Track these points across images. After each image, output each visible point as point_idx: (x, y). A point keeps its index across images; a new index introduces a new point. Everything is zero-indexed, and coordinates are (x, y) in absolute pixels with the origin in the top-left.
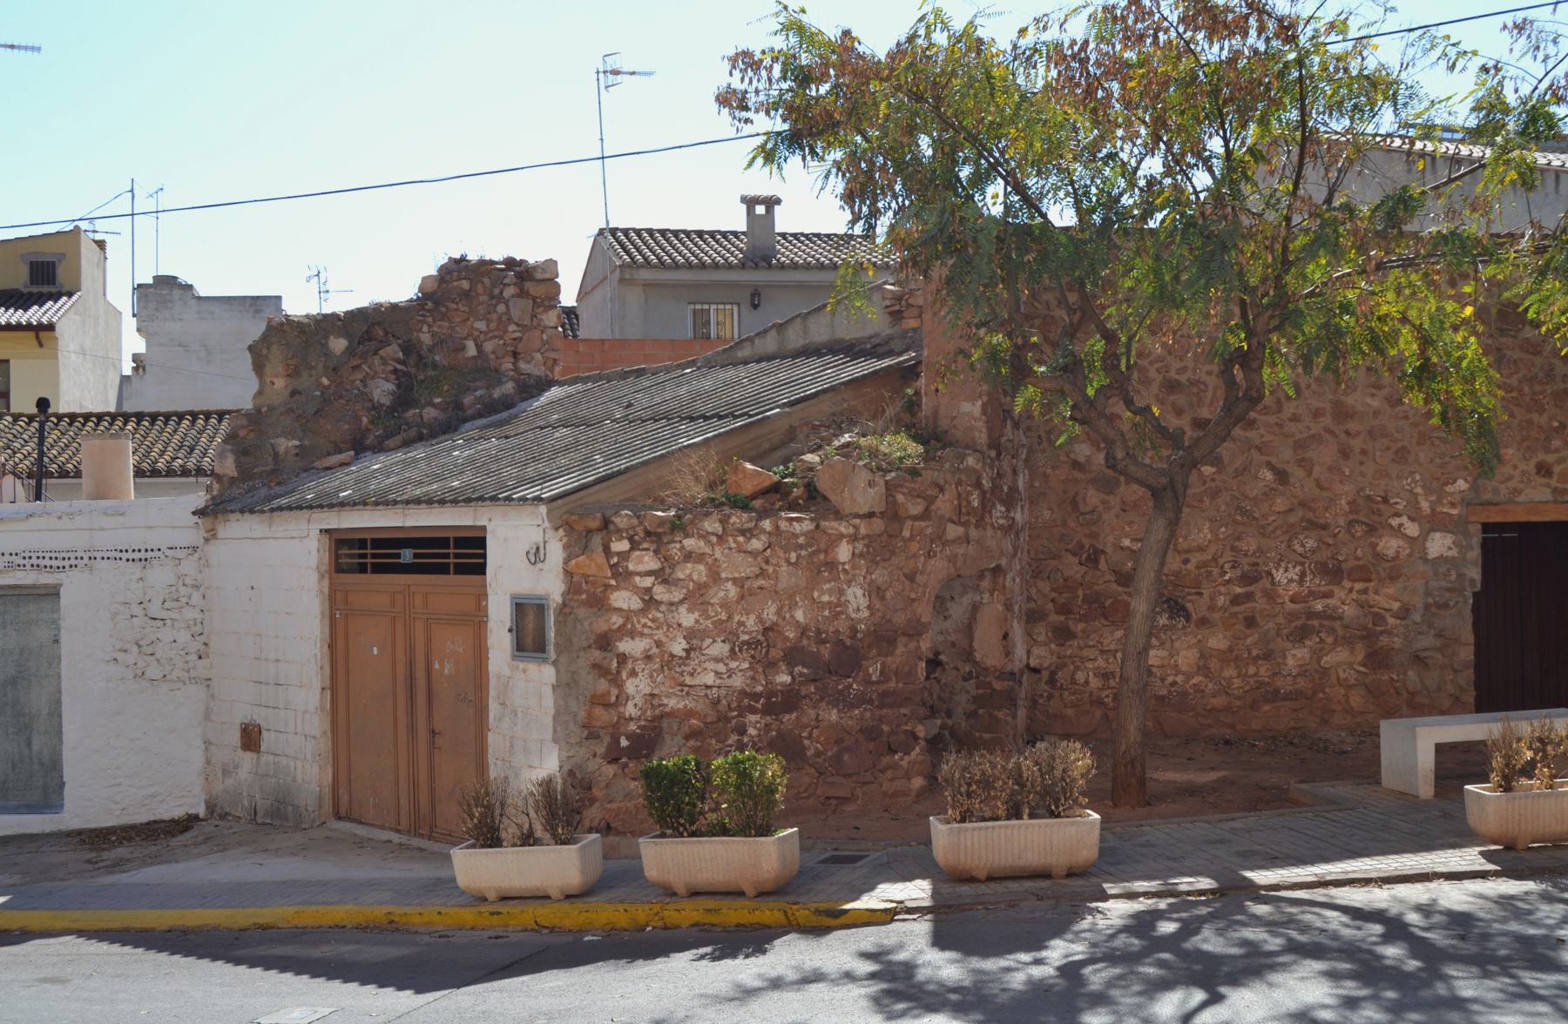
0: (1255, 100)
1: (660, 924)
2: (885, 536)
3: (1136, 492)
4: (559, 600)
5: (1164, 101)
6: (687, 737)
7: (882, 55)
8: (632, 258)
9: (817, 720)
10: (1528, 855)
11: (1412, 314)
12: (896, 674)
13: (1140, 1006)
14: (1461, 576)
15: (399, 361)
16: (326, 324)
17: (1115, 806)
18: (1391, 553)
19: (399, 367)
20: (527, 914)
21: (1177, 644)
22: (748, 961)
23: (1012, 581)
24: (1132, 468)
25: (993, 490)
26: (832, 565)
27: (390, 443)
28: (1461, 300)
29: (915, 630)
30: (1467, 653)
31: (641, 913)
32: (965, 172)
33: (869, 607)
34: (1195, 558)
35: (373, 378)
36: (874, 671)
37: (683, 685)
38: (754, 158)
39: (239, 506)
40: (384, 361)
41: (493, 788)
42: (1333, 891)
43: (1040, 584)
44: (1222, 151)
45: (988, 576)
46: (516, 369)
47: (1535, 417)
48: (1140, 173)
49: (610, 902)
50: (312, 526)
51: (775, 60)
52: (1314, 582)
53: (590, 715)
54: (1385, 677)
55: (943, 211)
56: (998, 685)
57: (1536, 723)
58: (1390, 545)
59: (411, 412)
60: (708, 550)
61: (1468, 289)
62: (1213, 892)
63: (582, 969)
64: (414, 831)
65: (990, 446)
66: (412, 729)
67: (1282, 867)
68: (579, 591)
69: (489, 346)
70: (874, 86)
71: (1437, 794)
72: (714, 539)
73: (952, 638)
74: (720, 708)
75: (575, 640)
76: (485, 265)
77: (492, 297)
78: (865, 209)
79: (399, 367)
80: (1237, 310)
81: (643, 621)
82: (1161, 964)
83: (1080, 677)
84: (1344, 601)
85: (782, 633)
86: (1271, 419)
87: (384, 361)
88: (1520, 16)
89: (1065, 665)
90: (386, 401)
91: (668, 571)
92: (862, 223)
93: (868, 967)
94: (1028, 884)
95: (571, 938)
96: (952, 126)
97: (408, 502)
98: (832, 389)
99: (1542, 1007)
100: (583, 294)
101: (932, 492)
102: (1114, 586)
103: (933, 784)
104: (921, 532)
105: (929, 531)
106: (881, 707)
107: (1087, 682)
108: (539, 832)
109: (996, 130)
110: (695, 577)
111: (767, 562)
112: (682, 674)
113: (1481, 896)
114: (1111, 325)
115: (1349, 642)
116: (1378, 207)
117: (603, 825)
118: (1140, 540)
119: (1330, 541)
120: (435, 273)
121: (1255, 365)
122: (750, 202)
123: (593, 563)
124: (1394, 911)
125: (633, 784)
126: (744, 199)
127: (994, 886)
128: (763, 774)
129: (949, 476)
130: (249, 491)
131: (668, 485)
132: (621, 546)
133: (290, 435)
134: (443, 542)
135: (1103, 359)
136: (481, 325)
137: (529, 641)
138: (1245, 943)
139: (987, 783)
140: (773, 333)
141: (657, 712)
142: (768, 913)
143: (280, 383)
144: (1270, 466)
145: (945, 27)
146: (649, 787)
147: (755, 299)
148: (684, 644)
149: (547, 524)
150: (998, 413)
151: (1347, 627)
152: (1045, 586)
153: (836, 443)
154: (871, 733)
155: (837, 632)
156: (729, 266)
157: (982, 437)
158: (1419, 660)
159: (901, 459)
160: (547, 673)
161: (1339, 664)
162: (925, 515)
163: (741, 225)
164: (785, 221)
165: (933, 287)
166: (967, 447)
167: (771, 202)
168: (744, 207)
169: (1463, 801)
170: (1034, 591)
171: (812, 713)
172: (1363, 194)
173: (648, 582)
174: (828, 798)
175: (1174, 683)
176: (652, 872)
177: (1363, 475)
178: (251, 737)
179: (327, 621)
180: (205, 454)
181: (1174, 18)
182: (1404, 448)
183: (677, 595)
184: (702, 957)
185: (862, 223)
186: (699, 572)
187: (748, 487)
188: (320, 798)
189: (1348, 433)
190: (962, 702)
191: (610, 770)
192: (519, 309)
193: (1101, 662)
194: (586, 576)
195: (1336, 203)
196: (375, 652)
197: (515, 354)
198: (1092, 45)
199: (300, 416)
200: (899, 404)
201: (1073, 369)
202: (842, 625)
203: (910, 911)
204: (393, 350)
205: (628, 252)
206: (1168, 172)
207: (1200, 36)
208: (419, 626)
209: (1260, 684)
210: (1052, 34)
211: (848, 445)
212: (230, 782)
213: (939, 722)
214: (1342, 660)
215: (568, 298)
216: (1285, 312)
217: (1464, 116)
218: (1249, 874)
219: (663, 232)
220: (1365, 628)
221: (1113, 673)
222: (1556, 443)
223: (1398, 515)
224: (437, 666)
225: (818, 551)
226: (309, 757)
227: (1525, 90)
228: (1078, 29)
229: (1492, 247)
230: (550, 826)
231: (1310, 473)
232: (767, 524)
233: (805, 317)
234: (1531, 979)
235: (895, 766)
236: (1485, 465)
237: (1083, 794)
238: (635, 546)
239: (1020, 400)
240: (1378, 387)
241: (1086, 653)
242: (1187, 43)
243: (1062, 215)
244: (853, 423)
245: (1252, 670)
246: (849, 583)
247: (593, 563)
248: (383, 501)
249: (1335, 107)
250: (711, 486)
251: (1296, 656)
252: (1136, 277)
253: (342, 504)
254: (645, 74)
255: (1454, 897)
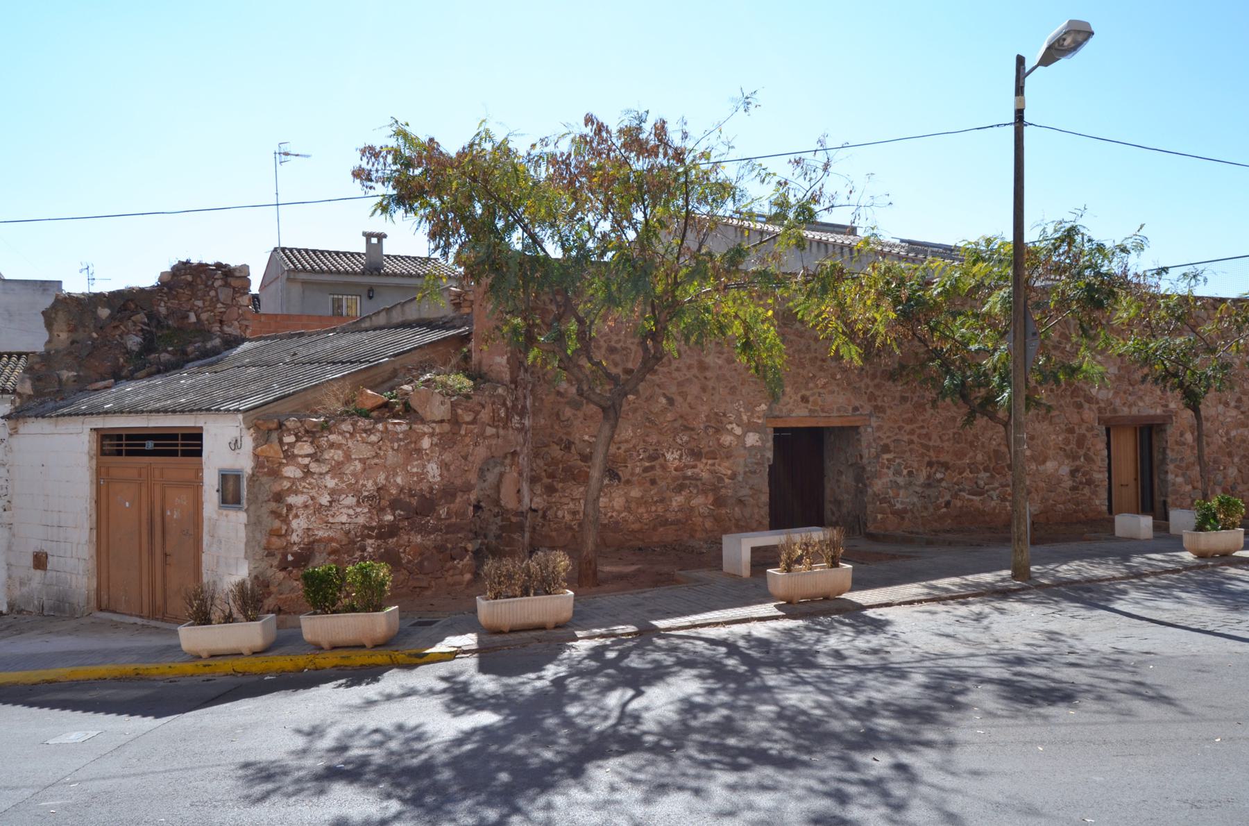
0: (663, 192)
1: (313, 667)
2: (450, 434)
3: (592, 409)
4: (250, 472)
5: (612, 190)
6: (329, 554)
7: (453, 154)
8: (295, 266)
9: (409, 541)
10: (799, 606)
11: (741, 314)
12: (456, 514)
13: (598, 700)
14: (762, 456)
15: (144, 324)
16: (96, 300)
17: (580, 586)
18: (727, 444)
19: (145, 327)
20: (227, 665)
21: (613, 495)
22: (368, 686)
23: (523, 460)
24: (592, 396)
25: (512, 408)
26: (419, 451)
27: (138, 374)
28: (767, 307)
29: (468, 488)
30: (765, 498)
31: (301, 661)
32: (500, 224)
33: (440, 475)
34: (624, 447)
35: (127, 334)
36: (443, 512)
37: (327, 522)
38: (375, 210)
39: (34, 413)
40: (135, 324)
41: (206, 588)
42: (700, 630)
43: (538, 461)
44: (642, 220)
45: (509, 457)
46: (222, 331)
47: (801, 371)
48: (597, 230)
49: (281, 655)
50: (85, 426)
51: (388, 152)
52: (687, 460)
53: (269, 542)
54: (723, 512)
55: (489, 246)
56: (514, 519)
57: (803, 535)
58: (727, 439)
59: (153, 356)
60: (344, 442)
61: (770, 301)
62: (635, 633)
63: (264, 697)
64: (152, 615)
65: (512, 382)
66: (151, 553)
67: (672, 618)
68: (262, 467)
69: (204, 316)
70: (449, 171)
71: (751, 575)
72: (348, 435)
73: (488, 492)
74: (350, 535)
75: (260, 496)
76: (202, 267)
77: (207, 286)
78: (442, 242)
79: (145, 327)
80: (649, 309)
81: (303, 484)
82: (608, 676)
83: (560, 514)
84: (703, 470)
85: (388, 491)
86: (665, 369)
87: (135, 324)
88: (798, 156)
89: (551, 508)
90: (136, 348)
91: (319, 454)
92: (440, 250)
93: (443, 685)
94: (533, 634)
95: (256, 678)
96: (494, 197)
97: (151, 412)
98: (420, 347)
99: (810, 688)
100: (263, 286)
101: (478, 408)
102: (579, 462)
103: (477, 576)
104: (471, 431)
105: (476, 431)
106: (447, 533)
107: (564, 517)
108: (236, 614)
109: (518, 201)
110: (336, 458)
111: (380, 449)
112: (327, 516)
113: (776, 629)
114: (581, 314)
115: (704, 492)
116: (725, 255)
117: (276, 608)
118: (595, 437)
119: (696, 437)
120: (169, 270)
121: (659, 339)
122: (368, 236)
123: (273, 450)
124: (731, 639)
125: (295, 583)
126: (364, 234)
127: (513, 636)
128: (377, 574)
129: (488, 400)
130: (41, 404)
131: (320, 403)
132: (290, 439)
133: (69, 368)
134: (175, 437)
135: (577, 334)
136: (199, 303)
137: (230, 497)
138: (654, 661)
139: (510, 576)
140: (384, 313)
141: (311, 539)
142: (380, 657)
143: (63, 336)
144: (665, 395)
145: (491, 139)
146: (307, 585)
147: (371, 293)
148: (328, 498)
149: (243, 426)
150: (517, 364)
151: (704, 484)
152: (541, 463)
153: (422, 379)
154: (440, 549)
155: (421, 489)
156: (355, 273)
157: (507, 377)
158: (740, 502)
159: (460, 389)
160: (242, 517)
161: (700, 505)
162: (474, 422)
163: (362, 249)
164: (389, 248)
165: (481, 290)
166: (498, 382)
167: (381, 237)
168: (364, 238)
169: (766, 578)
170: (534, 465)
171: (406, 538)
172: (718, 247)
173: (306, 461)
174: (415, 587)
175: (612, 517)
176: (308, 635)
177: (713, 401)
178: (40, 561)
179: (94, 486)
180: (8, 380)
181: (619, 144)
182: (734, 387)
183: (324, 469)
184: (340, 686)
185: (440, 250)
186: (338, 455)
187: (369, 404)
188: (88, 598)
189: (705, 378)
190: (493, 529)
191: (281, 575)
192: (225, 294)
193: (571, 505)
194: (267, 458)
195: (703, 251)
196: (127, 504)
197: (221, 322)
198: (573, 157)
199: (77, 357)
200: (459, 357)
201: (560, 338)
202: (424, 486)
203: (465, 652)
204: (141, 317)
205: (292, 262)
206: (613, 230)
207: (633, 155)
208: (157, 489)
209: (658, 516)
210: (550, 149)
211: (428, 380)
212: (25, 590)
213: (479, 541)
214: (701, 502)
215: (255, 289)
216: (674, 308)
217: (766, 209)
218: (654, 623)
219: (314, 251)
220: (714, 485)
221: (578, 512)
222: (811, 385)
223: (731, 423)
224: (169, 513)
225: (411, 442)
226: (81, 572)
227: (800, 195)
228: (565, 147)
229: (782, 280)
230: (244, 611)
231: (685, 399)
232: (380, 426)
233: (403, 304)
234: (802, 673)
235: (455, 568)
236: (774, 398)
237: (564, 580)
238: (298, 439)
239: (531, 357)
240: (721, 353)
241: (565, 500)
242: (626, 159)
243: (554, 251)
244: (432, 367)
245: (653, 509)
246: (429, 461)
247: (273, 450)
248: (134, 411)
249: (703, 200)
250: (347, 403)
251: (677, 500)
252: (595, 287)
253: (106, 413)
254: (305, 156)
255: (760, 630)
